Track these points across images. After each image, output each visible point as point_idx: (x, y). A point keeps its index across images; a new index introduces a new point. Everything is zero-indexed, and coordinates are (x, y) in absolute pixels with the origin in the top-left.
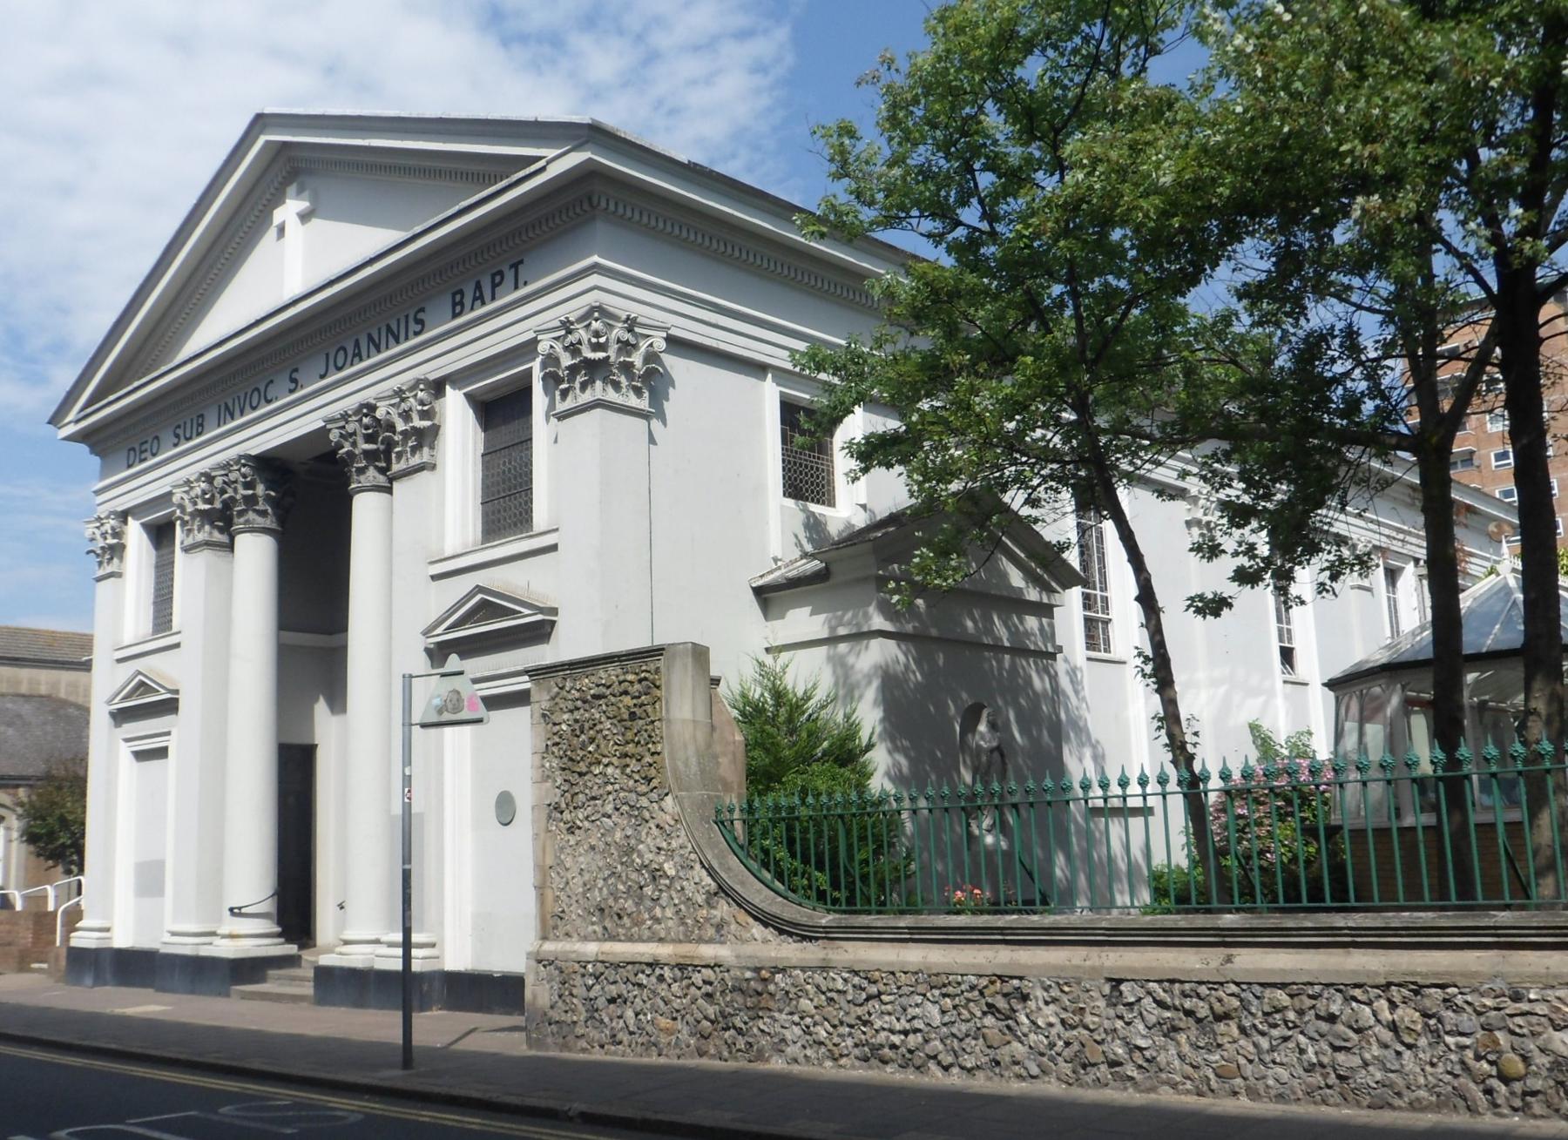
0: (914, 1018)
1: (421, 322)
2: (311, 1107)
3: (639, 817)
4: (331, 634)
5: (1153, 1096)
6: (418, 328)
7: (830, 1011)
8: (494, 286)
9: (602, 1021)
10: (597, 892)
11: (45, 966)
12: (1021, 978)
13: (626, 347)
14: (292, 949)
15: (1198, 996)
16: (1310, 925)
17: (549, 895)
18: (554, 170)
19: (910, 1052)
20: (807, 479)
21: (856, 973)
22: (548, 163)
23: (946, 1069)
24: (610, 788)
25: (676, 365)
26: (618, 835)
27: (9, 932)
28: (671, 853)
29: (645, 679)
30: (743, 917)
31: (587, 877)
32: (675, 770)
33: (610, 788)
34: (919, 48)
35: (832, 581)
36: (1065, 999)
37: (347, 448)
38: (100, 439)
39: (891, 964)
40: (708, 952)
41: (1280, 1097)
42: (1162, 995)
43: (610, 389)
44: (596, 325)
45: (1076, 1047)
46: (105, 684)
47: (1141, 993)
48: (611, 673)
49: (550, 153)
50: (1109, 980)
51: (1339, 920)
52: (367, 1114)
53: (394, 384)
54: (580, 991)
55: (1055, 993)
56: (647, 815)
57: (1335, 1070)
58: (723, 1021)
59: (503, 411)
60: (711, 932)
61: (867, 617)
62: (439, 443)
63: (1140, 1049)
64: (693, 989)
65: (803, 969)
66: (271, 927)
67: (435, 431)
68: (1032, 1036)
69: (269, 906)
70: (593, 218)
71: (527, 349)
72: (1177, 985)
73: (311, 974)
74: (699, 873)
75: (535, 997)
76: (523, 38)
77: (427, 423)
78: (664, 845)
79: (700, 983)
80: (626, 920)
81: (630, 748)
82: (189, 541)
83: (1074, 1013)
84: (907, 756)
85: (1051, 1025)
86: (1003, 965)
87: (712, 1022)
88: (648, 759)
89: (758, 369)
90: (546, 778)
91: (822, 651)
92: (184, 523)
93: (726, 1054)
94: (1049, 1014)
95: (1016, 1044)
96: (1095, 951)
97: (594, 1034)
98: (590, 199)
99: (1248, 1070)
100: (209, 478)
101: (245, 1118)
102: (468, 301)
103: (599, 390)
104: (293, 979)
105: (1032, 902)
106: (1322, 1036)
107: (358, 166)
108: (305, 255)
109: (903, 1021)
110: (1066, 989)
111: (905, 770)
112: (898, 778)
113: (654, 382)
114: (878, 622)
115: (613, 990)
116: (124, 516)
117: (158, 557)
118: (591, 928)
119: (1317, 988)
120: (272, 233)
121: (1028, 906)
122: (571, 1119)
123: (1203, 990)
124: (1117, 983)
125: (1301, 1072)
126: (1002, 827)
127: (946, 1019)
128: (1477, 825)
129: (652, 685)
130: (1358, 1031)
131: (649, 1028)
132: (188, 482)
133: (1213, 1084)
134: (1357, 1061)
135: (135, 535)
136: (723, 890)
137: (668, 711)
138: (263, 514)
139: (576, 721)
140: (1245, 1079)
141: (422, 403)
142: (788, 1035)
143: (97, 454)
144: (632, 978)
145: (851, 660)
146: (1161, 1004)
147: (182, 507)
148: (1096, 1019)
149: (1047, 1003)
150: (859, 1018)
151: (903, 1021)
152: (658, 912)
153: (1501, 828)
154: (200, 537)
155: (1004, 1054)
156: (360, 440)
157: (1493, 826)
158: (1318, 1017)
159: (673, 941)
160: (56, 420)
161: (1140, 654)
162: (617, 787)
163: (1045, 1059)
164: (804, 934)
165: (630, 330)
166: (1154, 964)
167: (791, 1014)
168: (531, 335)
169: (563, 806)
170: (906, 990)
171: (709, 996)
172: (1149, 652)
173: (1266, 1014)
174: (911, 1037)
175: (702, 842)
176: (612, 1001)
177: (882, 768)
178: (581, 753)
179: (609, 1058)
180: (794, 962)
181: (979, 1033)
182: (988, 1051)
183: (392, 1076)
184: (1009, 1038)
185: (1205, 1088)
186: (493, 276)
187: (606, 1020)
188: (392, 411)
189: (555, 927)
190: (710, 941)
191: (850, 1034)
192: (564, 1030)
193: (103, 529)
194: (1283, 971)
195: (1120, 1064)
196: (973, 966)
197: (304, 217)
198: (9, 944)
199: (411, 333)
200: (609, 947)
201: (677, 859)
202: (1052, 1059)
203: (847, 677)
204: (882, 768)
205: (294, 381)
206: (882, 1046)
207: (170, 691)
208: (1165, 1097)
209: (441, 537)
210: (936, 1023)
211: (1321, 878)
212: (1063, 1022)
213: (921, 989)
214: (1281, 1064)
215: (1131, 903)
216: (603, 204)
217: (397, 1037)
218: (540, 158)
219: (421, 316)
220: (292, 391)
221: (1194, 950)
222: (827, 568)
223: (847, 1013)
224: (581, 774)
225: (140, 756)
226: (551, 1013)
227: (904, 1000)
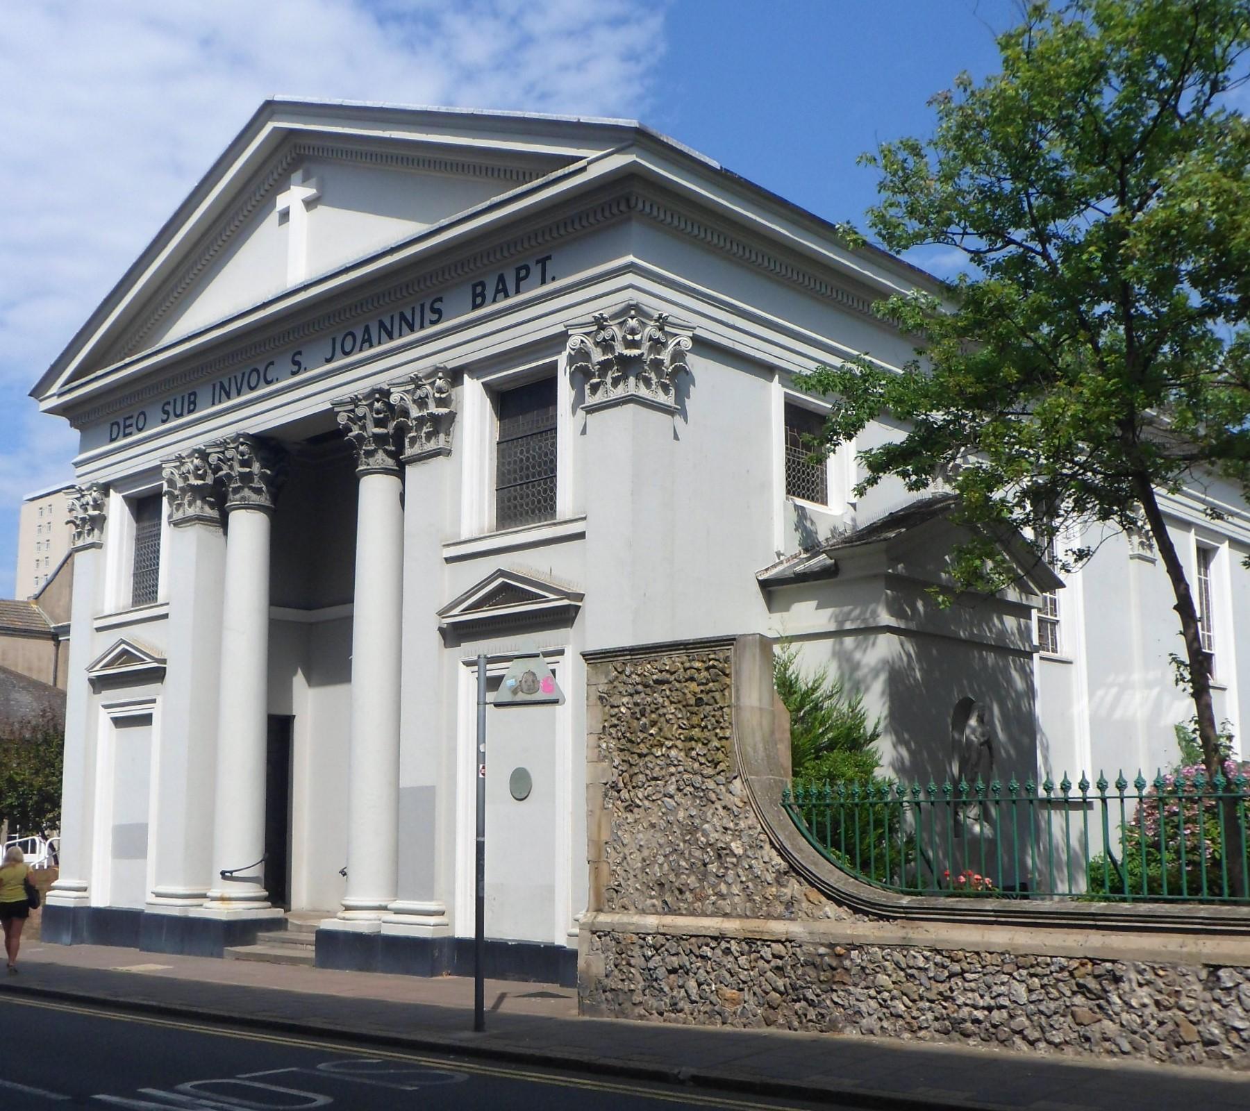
0: (999, 995)
1: (439, 312)
2: (407, 1066)
6: (435, 317)
7: (910, 986)
8: (519, 280)
9: (661, 990)
10: (657, 868)
12: (1113, 962)
13: (657, 345)
14: (278, 913)
17: (605, 869)
18: (595, 171)
19: (995, 1026)
20: (805, 479)
21: (939, 952)
22: (589, 163)
23: (1032, 1043)
24: (673, 769)
25: (698, 365)
26: (681, 815)
28: (738, 834)
29: (714, 667)
30: (815, 895)
33: (673, 769)
34: (989, 72)
35: (839, 578)
36: (1160, 982)
37: (356, 431)
39: (977, 944)
40: (779, 928)
43: (641, 385)
44: (632, 323)
45: (1170, 1026)
46: (86, 651)
50: (1206, 966)
53: (411, 370)
54: (638, 961)
55: (1149, 976)
56: (713, 797)
58: (794, 993)
59: (524, 402)
60: (780, 909)
61: (874, 614)
62: (456, 428)
63: (1238, 1030)
65: (881, 947)
66: (257, 890)
68: (1125, 1016)
69: (257, 872)
70: (629, 219)
73: (313, 937)
74: (769, 853)
75: (588, 965)
76: (398, 17)
78: (731, 825)
79: (770, 957)
80: (688, 895)
81: (696, 732)
82: (178, 515)
83: (1169, 995)
84: (909, 750)
85: (1145, 1006)
86: (1096, 949)
87: (781, 994)
88: (716, 743)
89: (766, 370)
90: (601, 759)
91: (828, 643)
92: (173, 497)
93: (796, 1024)
94: (1144, 995)
95: (1107, 1023)
96: (1190, 938)
97: (653, 1002)
98: (628, 201)
100: (204, 455)
101: (350, 1074)
102: (490, 293)
103: (632, 386)
105: (1013, 888)
107: (372, 156)
108: (306, 244)
109: (987, 998)
110: (1161, 973)
111: (907, 762)
112: (900, 768)
113: (679, 380)
114: (885, 618)
115: (675, 961)
116: (105, 488)
117: (138, 529)
118: (649, 902)
120: (274, 217)
122: (682, 1082)
124: (1214, 969)
126: (985, 816)
127: (1034, 997)
129: (720, 674)
131: (714, 998)
132: (180, 458)
135: (116, 507)
136: (795, 869)
137: (738, 698)
138: (258, 491)
139: (636, 704)
143: (76, 428)
145: (858, 656)
147: (171, 483)
148: (1192, 1002)
150: (940, 994)
151: (987, 998)
152: (723, 888)
154: (191, 512)
155: (1094, 1031)
159: (739, 916)
160: (38, 392)
162: (681, 769)
163: (1137, 1037)
164: (881, 913)
165: (661, 329)
167: (867, 988)
168: (561, 328)
169: (621, 785)
170: (990, 969)
171: (779, 970)
172: (1185, 657)
174: (995, 1013)
175: (774, 824)
176: (673, 971)
177: (886, 757)
178: (642, 736)
181: (1069, 1011)
182: (1077, 1028)
183: (466, 1037)
184: (1100, 1016)
186: (518, 270)
187: (666, 989)
188: (408, 398)
189: (611, 900)
191: (930, 1009)
193: (84, 500)
195: (1215, 1043)
196: (1064, 948)
197: (310, 204)
199: (426, 322)
200: (669, 920)
202: (1144, 1037)
204: (886, 757)
206: (964, 1020)
207: (156, 660)
210: (1024, 1000)
212: (1157, 1003)
213: (1007, 969)
215: (1070, 889)
216: (640, 206)
218: (581, 158)
219: (437, 306)
220: (294, 374)
222: (836, 564)
224: (641, 756)
225: (119, 722)
226: (605, 981)
227: (989, 979)
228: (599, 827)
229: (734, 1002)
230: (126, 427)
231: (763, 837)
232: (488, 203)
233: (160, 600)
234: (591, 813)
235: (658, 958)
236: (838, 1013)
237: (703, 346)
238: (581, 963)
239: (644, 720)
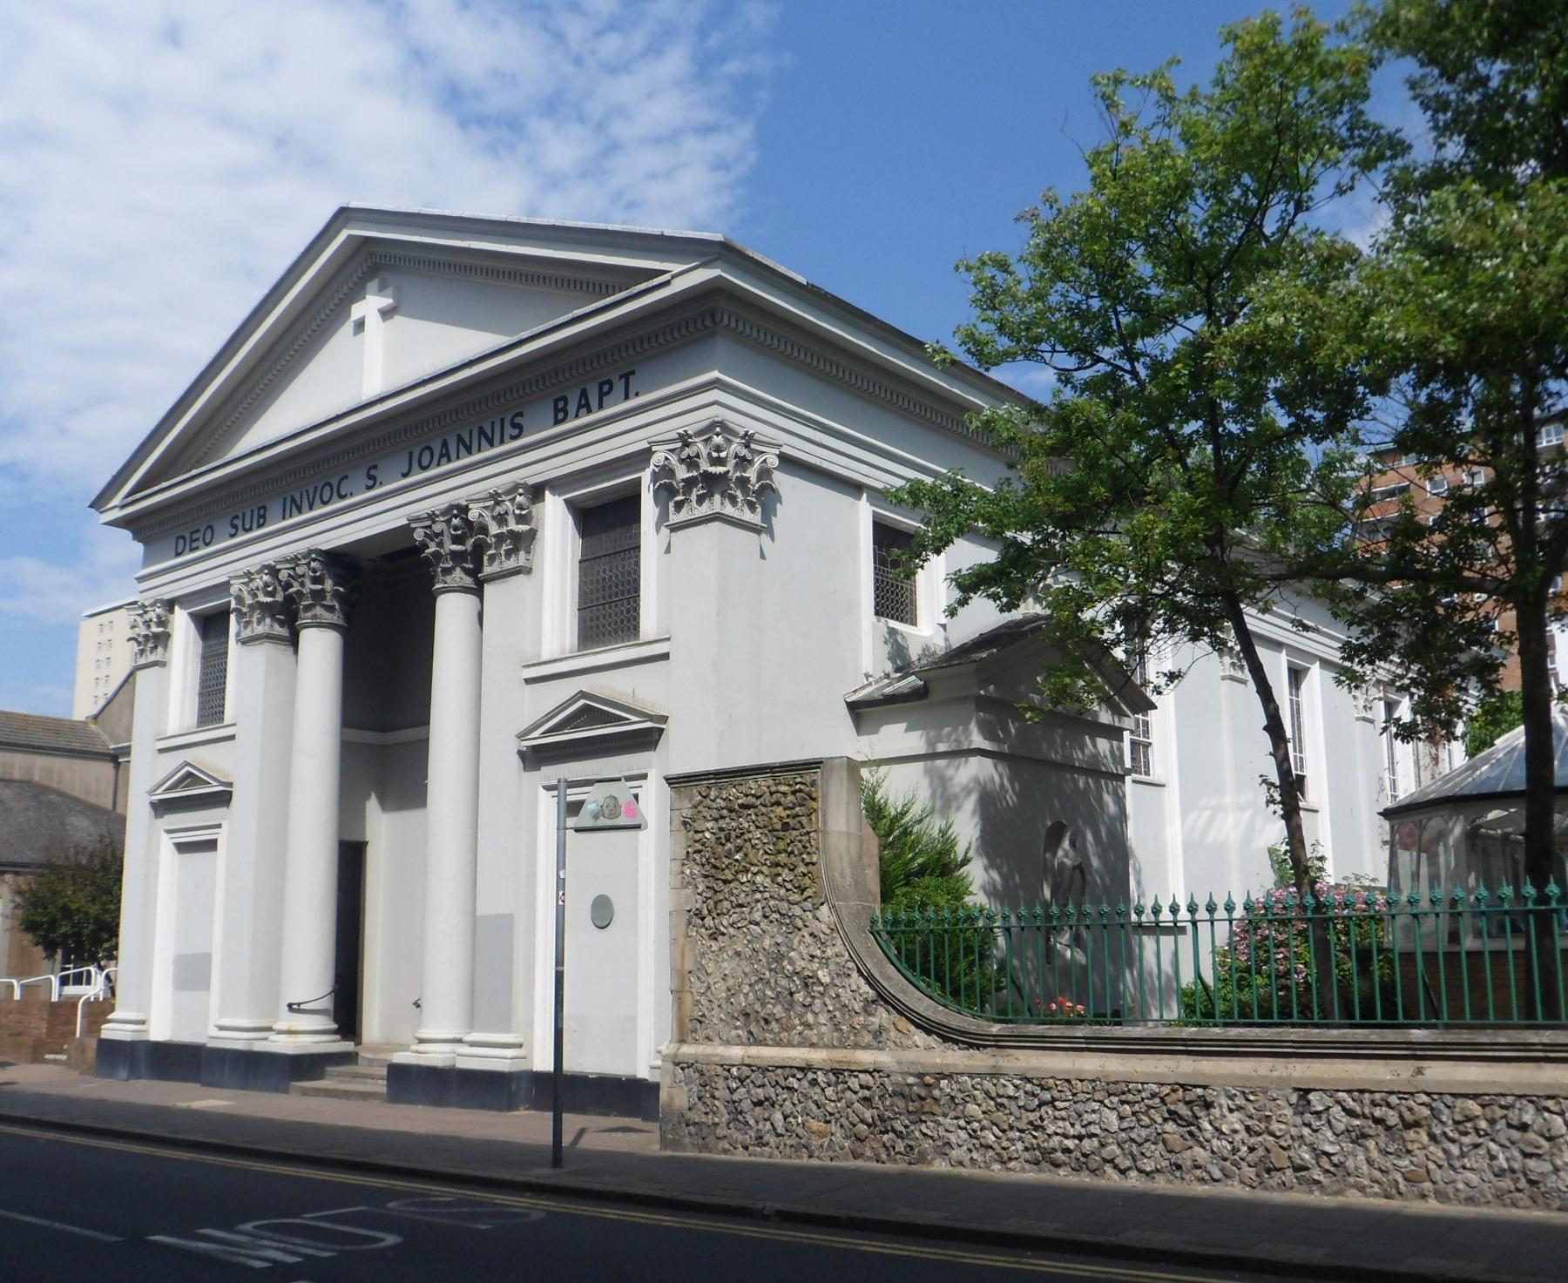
1: (520, 427)
2: (479, 1203)
3: (791, 925)
4: (384, 730)
5: (1340, 1198)
6: (516, 432)
7: (999, 1116)
8: (602, 395)
11: (64, 1057)
12: (1205, 1087)
13: (743, 462)
14: (348, 1046)
15: (1389, 1105)
16: (1503, 1040)
17: (688, 999)
18: (679, 285)
19: (1085, 1155)
20: (894, 599)
21: (1029, 1080)
22: (673, 277)
23: (1123, 1172)
24: (758, 896)
25: (784, 482)
26: (767, 942)
27: (19, 1022)
28: (825, 962)
29: (800, 791)
31: (731, 982)
32: (831, 881)
33: (758, 896)
34: (1076, 188)
36: (1250, 1107)
37: (432, 548)
38: (141, 526)
39: (1068, 1072)
40: (866, 1057)
41: (1470, 1200)
42: (1351, 1104)
43: (727, 502)
44: (718, 440)
45: (1261, 1152)
46: (147, 774)
47: (1329, 1102)
48: (763, 784)
49: (676, 268)
51: (1532, 1037)
52: (549, 1212)
53: (491, 486)
54: (722, 1093)
55: (1240, 1101)
56: (800, 923)
57: (1525, 1175)
58: (882, 1124)
59: (607, 519)
60: (868, 1038)
61: (967, 731)
63: (1328, 1155)
64: (848, 1094)
65: (971, 1076)
66: (326, 1023)
67: (532, 535)
68: (1215, 1142)
69: (327, 1003)
71: (641, 458)
72: (1367, 1095)
73: (384, 1071)
75: (671, 1098)
77: (523, 528)
78: (818, 953)
81: (782, 858)
82: (247, 633)
84: (1000, 873)
85: (1235, 1131)
86: (1187, 1075)
87: (869, 1125)
88: (802, 869)
89: (854, 488)
93: (884, 1156)
94: (1234, 1121)
95: (1197, 1149)
97: (737, 1136)
98: (713, 315)
99: (1438, 1175)
100: (273, 571)
103: (717, 504)
104: (355, 1076)
106: (1513, 1143)
107: (453, 267)
108: (383, 355)
109: (1078, 1126)
113: (766, 498)
114: (978, 741)
115: (760, 1093)
116: (170, 605)
117: (204, 648)
118: (734, 1033)
119: (1510, 1099)
120: (348, 327)
121: (1099, 1019)
123: (1393, 1099)
124: (1304, 1093)
125: (1492, 1177)
127: (1125, 1125)
128: (1563, 951)
129: (807, 798)
130: (1550, 1139)
131: (800, 1131)
132: (248, 574)
133: (1402, 1187)
134: (1547, 1167)
135: (182, 625)
136: (884, 998)
137: (825, 823)
138: (330, 609)
139: (721, 829)
140: (1434, 1183)
141: (520, 507)
142: (953, 1138)
144: (782, 1083)
146: (1350, 1113)
147: (239, 599)
149: (1231, 1111)
150: (1031, 1123)
151: (1078, 1126)
152: (810, 1018)
153: (1510, 955)
154: (260, 629)
155: (1185, 1158)
156: (447, 540)
157: (1481, 953)
158: (1510, 1126)
159: (826, 1046)
160: (98, 503)
161: (1264, 781)
162: (767, 895)
164: (971, 1042)
165: (747, 446)
166: (1344, 1075)
167: (957, 1118)
169: (705, 912)
170: (1081, 1097)
173: (1456, 1123)
174: (1086, 1142)
175: (862, 952)
176: (759, 1104)
178: (727, 861)
179: (753, 1159)
180: (961, 1069)
181: (1160, 1138)
182: (1168, 1156)
183: (544, 1174)
184: (1190, 1143)
185: (1394, 1191)
186: (601, 385)
187: (752, 1122)
188: (486, 514)
189: (694, 1031)
190: (868, 1047)
191: (1020, 1139)
192: (704, 1133)
193: (147, 617)
194: (1476, 1083)
195: (1307, 1169)
196: (1155, 1074)
197: (386, 314)
198: (20, 1034)
199: (506, 437)
200: (754, 1051)
201: (832, 967)
202: (1235, 1163)
203: (944, 789)
205: (373, 478)
207: (223, 784)
208: (1354, 1198)
209: (537, 640)
210: (1114, 1127)
211: (1373, 998)
212: (1248, 1129)
213: (1097, 1096)
214: (1471, 1169)
216: (726, 321)
217: (547, 1138)
218: (665, 272)
219: (517, 420)
220: (369, 488)
221: (1532, 1065)
222: (925, 685)
223: (1018, 1119)
224: (725, 882)
225: (182, 848)
226: (689, 1115)
227: (1080, 1107)
228: (683, 954)
229: (821, 1135)
230: (192, 541)
231: (850, 965)
232: (570, 316)
233: (227, 720)
234: (674, 941)
235: (743, 1090)
236: (927, 1144)
237: (790, 463)
238: (663, 1096)
239: (729, 845)
